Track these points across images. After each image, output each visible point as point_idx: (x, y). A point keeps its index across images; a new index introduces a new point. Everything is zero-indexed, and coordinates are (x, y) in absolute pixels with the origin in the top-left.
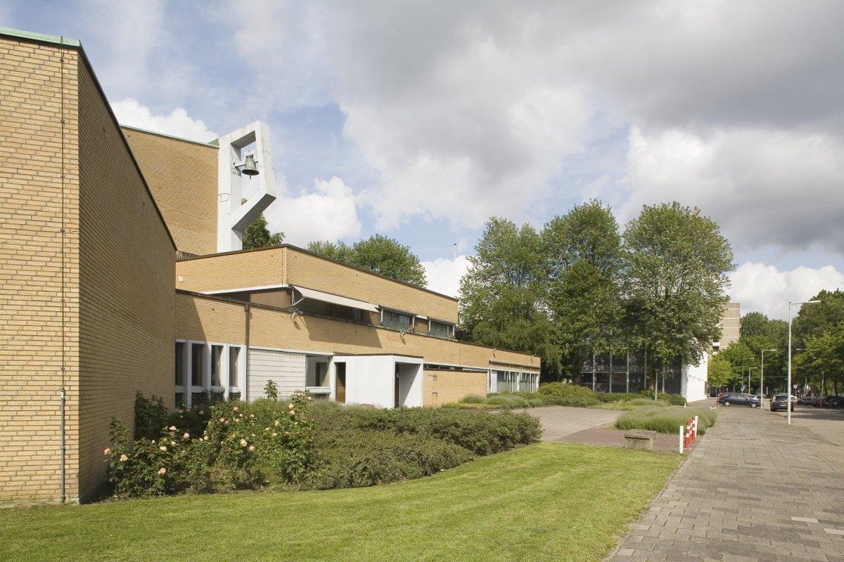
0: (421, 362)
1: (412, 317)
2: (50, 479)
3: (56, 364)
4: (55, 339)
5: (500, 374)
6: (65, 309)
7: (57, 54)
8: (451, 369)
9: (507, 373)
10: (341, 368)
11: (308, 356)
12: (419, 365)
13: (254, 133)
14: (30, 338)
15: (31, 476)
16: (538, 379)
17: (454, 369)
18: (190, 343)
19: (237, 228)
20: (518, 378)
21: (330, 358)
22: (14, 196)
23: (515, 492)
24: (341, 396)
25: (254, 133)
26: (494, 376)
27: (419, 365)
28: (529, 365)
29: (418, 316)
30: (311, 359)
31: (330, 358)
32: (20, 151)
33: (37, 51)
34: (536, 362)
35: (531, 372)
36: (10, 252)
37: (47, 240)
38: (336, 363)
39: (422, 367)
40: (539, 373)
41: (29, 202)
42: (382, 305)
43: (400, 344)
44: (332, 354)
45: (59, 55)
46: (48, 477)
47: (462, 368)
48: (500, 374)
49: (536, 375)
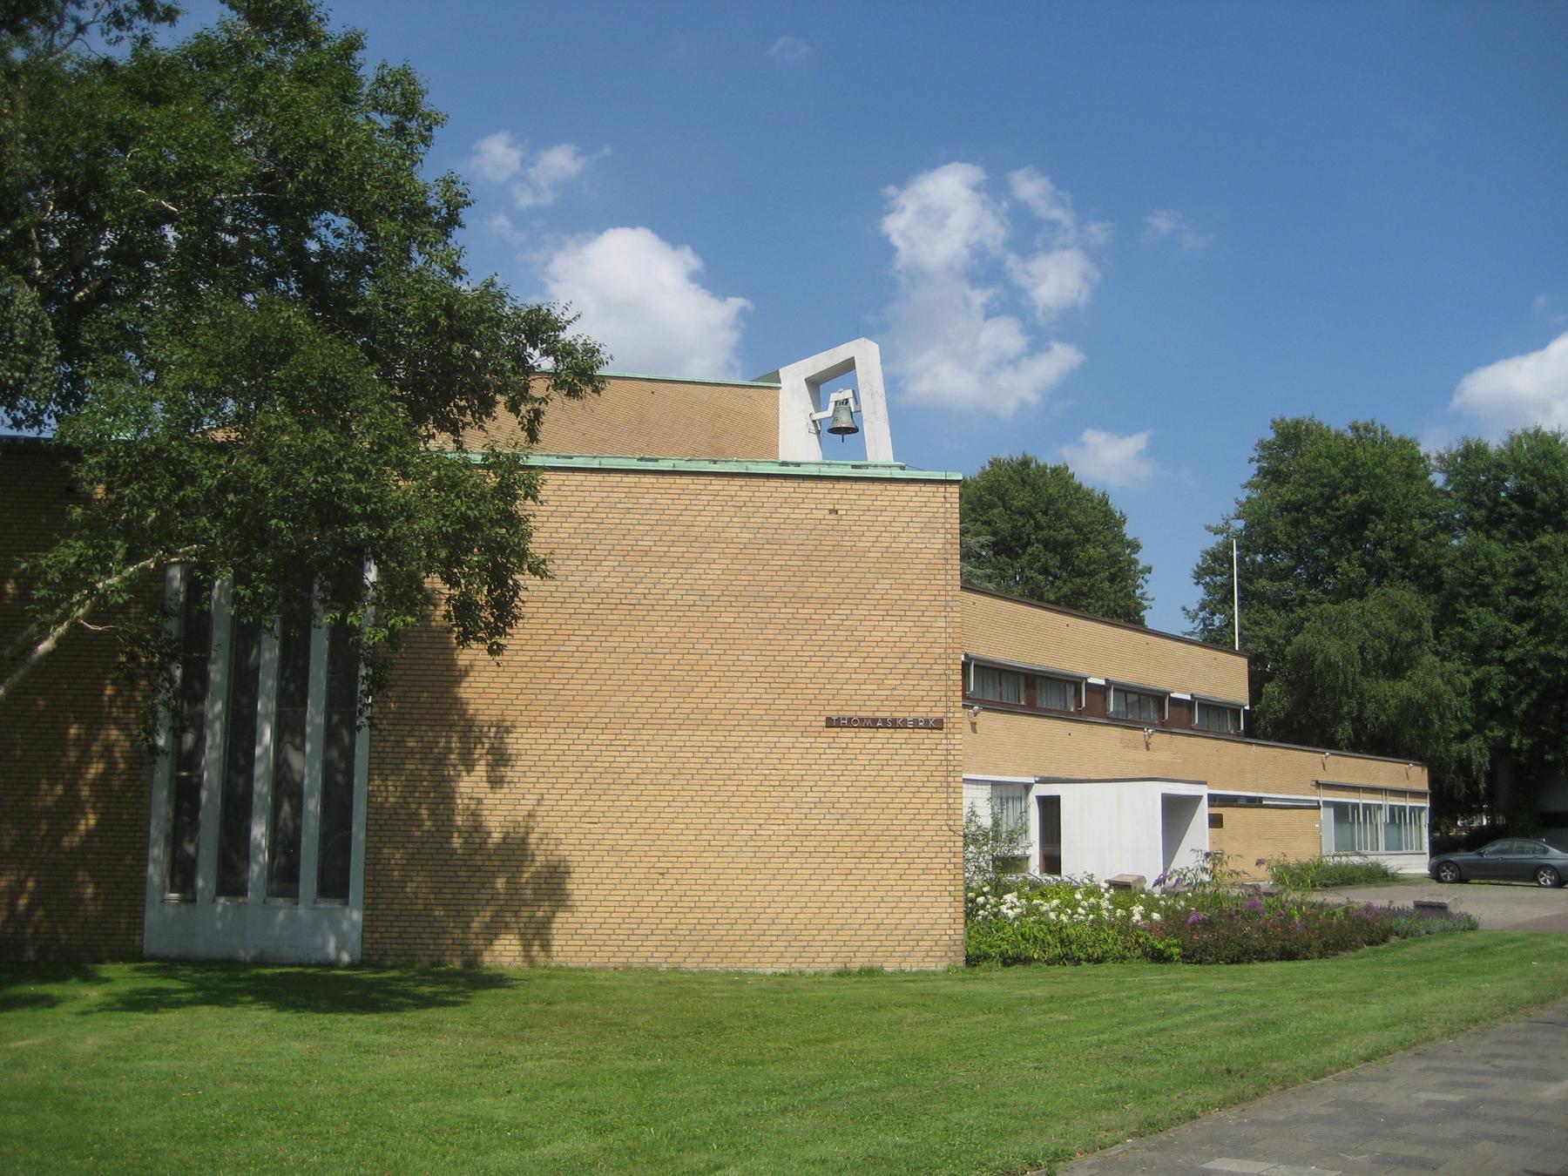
0: (1204, 791)
1: (1164, 699)
5: (1341, 811)
6: (945, 806)
9: (1356, 806)
10: (1050, 807)
11: (994, 784)
12: (1200, 797)
13: (852, 359)
16: (1425, 818)
17: (1244, 802)
20: (1382, 817)
21: (1028, 787)
25: (852, 359)
26: (1327, 815)
27: (1200, 797)
28: (1403, 786)
29: (1089, 681)
30: (999, 788)
31: (1028, 787)
34: (1418, 777)
35: (1409, 803)
39: (1205, 800)
40: (1426, 804)
42: (1111, 679)
43: (1143, 755)
44: (1031, 780)
46: (542, 881)
47: (1261, 799)
48: (1341, 811)
49: (1421, 809)
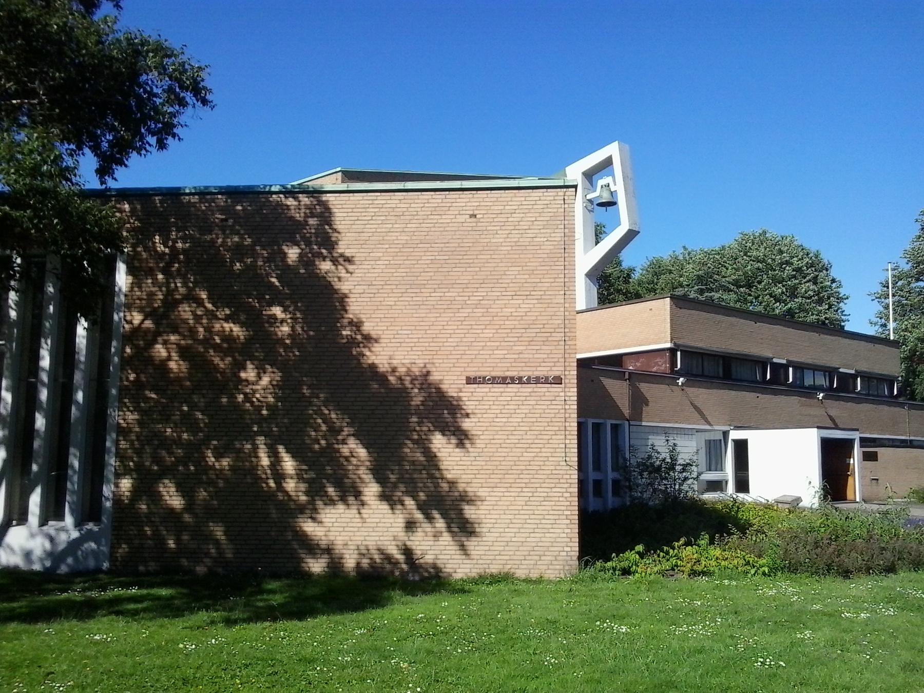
0: (856, 436)
2: (556, 560)
3: (559, 455)
4: (558, 433)
7: (560, 194)
8: (887, 443)
10: (741, 447)
14: (539, 432)
15: (540, 556)
18: (609, 422)
19: (589, 275)
22: (528, 314)
23: (158, 662)
24: (742, 485)
32: (533, 276)
33: (545, 194)
36: (524, 360)
37: (551, 348)
38: (734, 440)
41: (539, 318)
45: (562, 194)
